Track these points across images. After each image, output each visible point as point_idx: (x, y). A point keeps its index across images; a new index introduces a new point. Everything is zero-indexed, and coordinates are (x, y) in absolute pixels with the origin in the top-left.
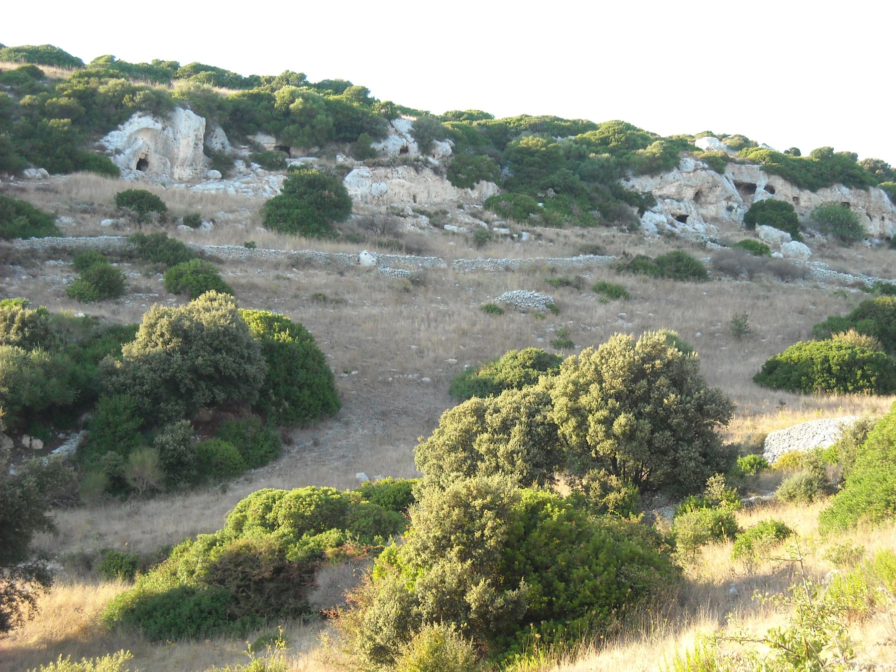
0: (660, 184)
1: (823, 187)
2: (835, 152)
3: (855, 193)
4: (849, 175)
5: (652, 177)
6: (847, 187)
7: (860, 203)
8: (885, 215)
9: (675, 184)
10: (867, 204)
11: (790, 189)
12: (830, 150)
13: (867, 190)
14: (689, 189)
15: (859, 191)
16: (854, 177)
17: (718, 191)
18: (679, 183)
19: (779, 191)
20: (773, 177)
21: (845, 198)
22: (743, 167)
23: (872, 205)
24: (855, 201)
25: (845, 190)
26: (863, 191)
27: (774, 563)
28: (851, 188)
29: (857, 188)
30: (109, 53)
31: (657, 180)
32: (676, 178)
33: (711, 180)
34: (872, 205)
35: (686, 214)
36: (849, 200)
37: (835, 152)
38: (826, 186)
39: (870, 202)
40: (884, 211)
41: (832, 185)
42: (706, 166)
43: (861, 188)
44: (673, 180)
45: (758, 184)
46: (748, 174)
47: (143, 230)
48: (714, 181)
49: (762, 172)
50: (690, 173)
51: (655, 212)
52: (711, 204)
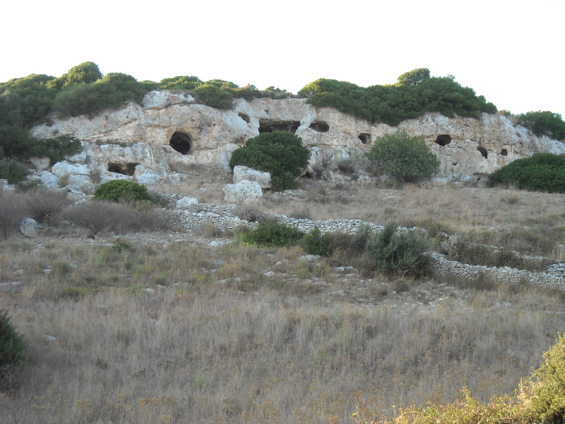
0: (105, 126)
1: (409, 118)
2: (431, 75)
3: (458, 122)
4: (445, 100)
5: (91, 118)
6: (445, 115)
7: (467, 135)
8: (507, 147)
9: (130, 125)
10: (479, 135)
11: (353, 123)
12: (425, 73)
13: (476, 117)
14: (158, 130)
15: (465, 119)
16: (454, 102)
17: (216, 131)
18: (137, 122)
19: (333, 128)
20: (324, 110)
21: (442, 129)
22: (283, 102)
23: (485, 135)
24: (459, 133)
25: (442, 120)
26: (471, 120)
27: (525, 156)
28: (452, 117)
29: (463, 116)
30: (411, 67)
31: (100, 121)
32: (130, 117)
33: (197, 116)
34: (485, 135)
35: (133, 162)
36: (448, 131)
37: (431, 75)
38: (413, 117)
39: (482, 132)
40: (505, 141)
41: (423, 115)
42: (191, 98)
43: (467, 116)
44: (126, 120)
45: (301, 121)
46: (290, 110)
47: (199, 158)
48: (203, 117)
49: (308, 105)
50: (158, 109)
51: (74, 163)
52: (206, 148)
